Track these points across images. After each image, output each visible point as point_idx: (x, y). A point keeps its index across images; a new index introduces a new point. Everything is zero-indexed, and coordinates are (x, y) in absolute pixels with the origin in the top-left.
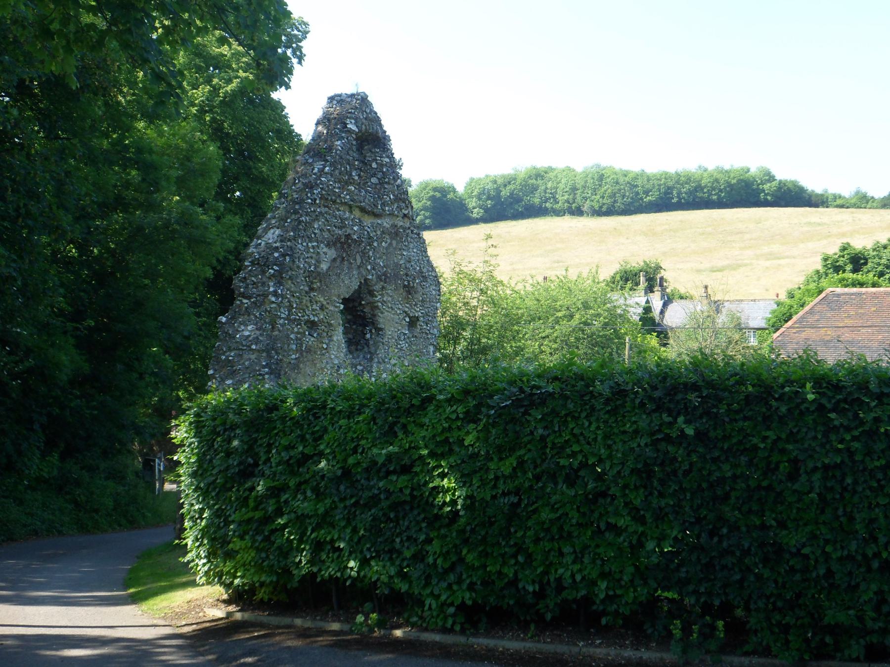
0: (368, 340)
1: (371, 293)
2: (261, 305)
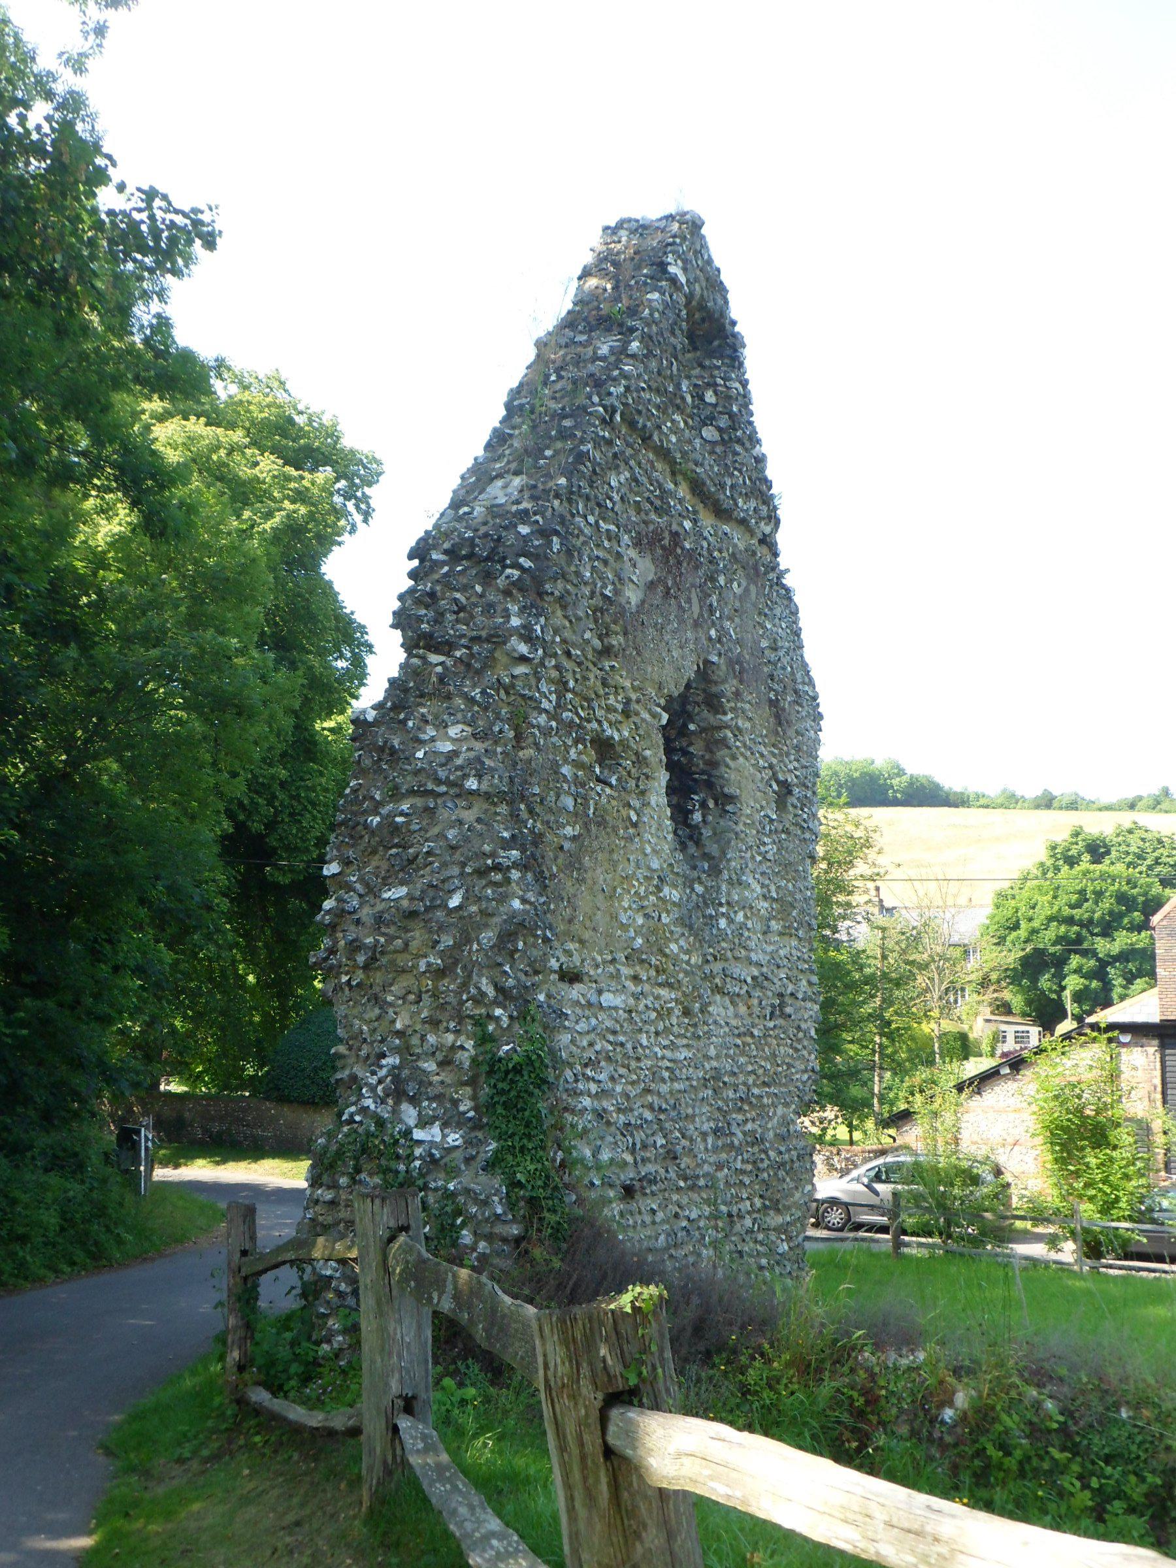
0: (696, 827)
1: (713, 703)
2: (485, 667)
